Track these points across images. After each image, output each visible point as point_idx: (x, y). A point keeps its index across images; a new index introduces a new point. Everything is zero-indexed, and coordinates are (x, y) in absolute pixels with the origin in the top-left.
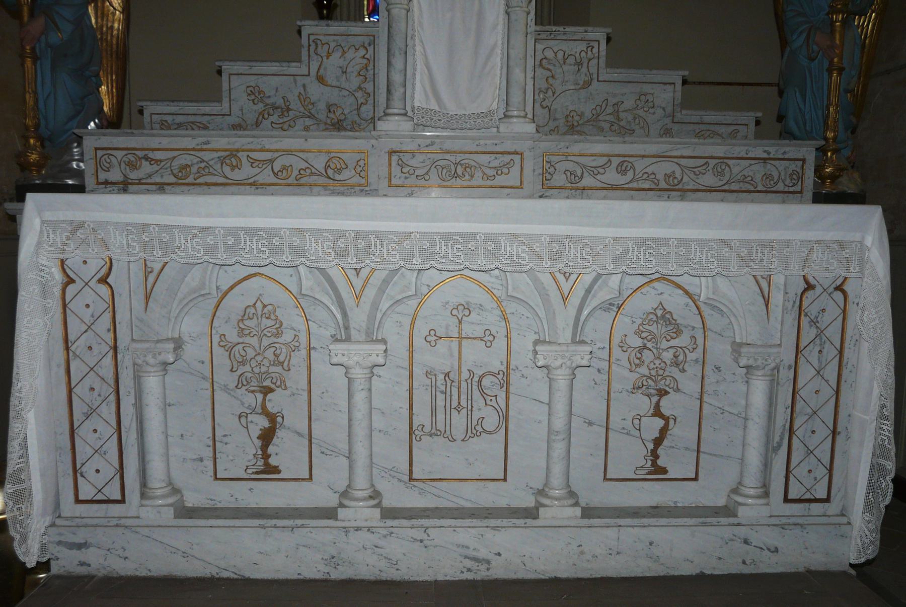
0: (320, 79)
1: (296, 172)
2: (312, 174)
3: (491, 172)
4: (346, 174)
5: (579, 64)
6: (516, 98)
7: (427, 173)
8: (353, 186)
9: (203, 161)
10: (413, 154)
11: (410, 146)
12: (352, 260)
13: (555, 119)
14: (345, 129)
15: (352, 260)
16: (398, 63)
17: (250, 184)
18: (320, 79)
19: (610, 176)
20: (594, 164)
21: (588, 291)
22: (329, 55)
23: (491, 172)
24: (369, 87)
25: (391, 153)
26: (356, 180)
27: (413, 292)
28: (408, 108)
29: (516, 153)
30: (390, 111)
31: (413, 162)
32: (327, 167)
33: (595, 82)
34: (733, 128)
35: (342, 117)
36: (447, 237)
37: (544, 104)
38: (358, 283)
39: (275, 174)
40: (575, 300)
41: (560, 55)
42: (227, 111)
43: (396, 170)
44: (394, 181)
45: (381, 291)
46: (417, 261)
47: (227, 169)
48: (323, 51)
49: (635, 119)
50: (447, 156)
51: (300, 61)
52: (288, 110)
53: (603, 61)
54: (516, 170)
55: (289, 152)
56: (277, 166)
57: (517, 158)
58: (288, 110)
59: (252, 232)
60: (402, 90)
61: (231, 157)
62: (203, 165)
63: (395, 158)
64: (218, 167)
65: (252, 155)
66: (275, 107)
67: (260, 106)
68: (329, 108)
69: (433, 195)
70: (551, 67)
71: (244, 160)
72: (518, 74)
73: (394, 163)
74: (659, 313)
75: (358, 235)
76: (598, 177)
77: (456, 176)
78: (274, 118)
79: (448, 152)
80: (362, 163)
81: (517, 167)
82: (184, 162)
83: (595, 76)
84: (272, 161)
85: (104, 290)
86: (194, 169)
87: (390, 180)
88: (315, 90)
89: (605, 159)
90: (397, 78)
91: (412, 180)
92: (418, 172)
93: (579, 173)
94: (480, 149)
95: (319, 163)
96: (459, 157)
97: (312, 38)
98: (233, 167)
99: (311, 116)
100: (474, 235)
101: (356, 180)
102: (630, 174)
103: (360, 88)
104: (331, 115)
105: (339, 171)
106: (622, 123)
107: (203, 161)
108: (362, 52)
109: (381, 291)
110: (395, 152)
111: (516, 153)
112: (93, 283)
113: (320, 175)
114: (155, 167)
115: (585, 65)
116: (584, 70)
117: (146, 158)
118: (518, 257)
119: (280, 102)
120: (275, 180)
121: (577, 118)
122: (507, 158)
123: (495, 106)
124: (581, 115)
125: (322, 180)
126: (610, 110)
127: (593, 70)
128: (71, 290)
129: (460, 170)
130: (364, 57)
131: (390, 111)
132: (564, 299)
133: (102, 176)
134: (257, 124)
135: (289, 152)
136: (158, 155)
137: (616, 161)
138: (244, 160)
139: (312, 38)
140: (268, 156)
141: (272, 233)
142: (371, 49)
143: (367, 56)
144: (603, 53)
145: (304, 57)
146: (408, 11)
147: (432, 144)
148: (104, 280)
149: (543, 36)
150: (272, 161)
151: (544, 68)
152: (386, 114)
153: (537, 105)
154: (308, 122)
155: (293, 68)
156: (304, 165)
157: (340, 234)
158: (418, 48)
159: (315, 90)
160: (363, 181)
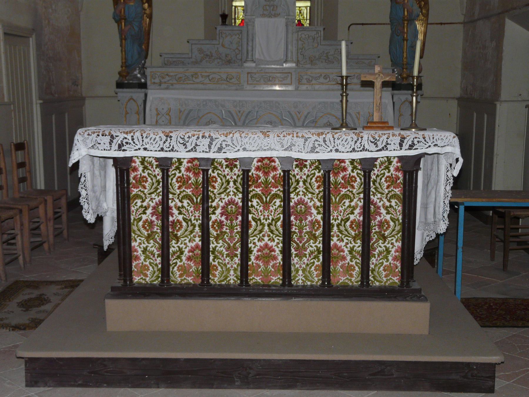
0: (223, 46)
1: (217, 80)
2: (222, 80)
3: (281, 79)
4: (233, 80)
5: (314, 39)
6: (289, 55)
7: (260, 80)
8: (235, 84)
9: (186, 76)
10: (255, 73)
11: (254, 71)
12: (238, 108)
13: (306, 59)
14: (232, 63)
15: (238, 108)
16: (250, 44)
17: (202, 84)
18: (223, 46)
19: (322, 80)
20: (316, 76)
21: (306, 117)
22: (226, 37)
23: (281, 79)
24: (240, 48)
25: (248, 73)
26: (237, 82)
27: (255, 117)
28: (254, 58)
29: (289, 73)
30: (248, 59)
31: (255, 76)
32: (227, 78)
33: (319, 45)
34: (369, 60)
35: (231, 59)
36: (265, 102)
37: (302, 53)
38: (240, 115)
39: (210, 80)
40: (302, 120)
41: (307, 36)
42: (190, 56)
43: (250, 78)
44: (249, 83)
45: (246, 117)
46: (256, 109)
47: (194, 79)
48: (224, 36)
49: (334, 58)
50: (267, 74)
51: (216, 40)
52: (212, 56)
53: (322, 38)
54: (289, 79)
55: (214, 73)
56: (211, 77)
57: (290, 75)
58: (212, 56)
59: (210, 101)
60: (252, 53)
61: (195, 75)
62: (186, 77)
63: (249, 75)
64: (191, 78)
65: (202, 74)
66: (207, 55)
67: (202, 55)
68: (226, 56)
69: (281, 362)
70: (304, 40)
71: (200, 76)
72: (290, 47)
73: (249, 76)
74: (328, 124)
75: (240, 101)
76: (318, 80)
77: (270, 80)
78: (207, 59)
79: (267, 73)
80: (238, 77)
81: (290, 78)
82: (179, 76)
83: (319, 43)
84: (209, 76)
85: (168, 117)
86: (183, 79)
87: (248, 82)
88: (221, 50)
89: (320, 75)
90: (250, 48)
91: (255, 82)
92: (257, 79)
93: (311, 79)
94: (277, 72)
95: (224, 77)
96: (271, 74)
97: (220, 31)
98: (196, 78)
99: (220, 59)
100: (272, 101)
101: (237, 82)
102: (328, 79)
103: (237, 49)
104: (227, 58)
105: (231, 79)
106: (329, 60)
107: (186, 76)
108: (238, 36)
109: (246, 117)
110: (250, 73)
111: (289, 73)
112: (165, 115)
113: (225, 80)
114: (171, 78)
115: (316, 39)
116: (316, 41)
117: (167, 75)
118: (285, 107)
119: (209, 53)
120: (210, 82)
121: (313, 58)
122: (286, 75)
123: (282, 57)
124: (315, 57)
125: (225, 82)
126: (325, 55)
127: (319, 41)
128: (159, 117)
129: (271, 79)
130: (238, 38)
131: (248, 59)
132: (299, 119)
133: (153, 81)
134: (201, 61)
135: (214, 73)
136: (171, 74)
137: (323, 75)
138: (200, 76)
139: (220, 31)
140: (208, 74)
141: (215, 101)
142: (241, 36)
143: (240, 37)
144: (322, 35)
145: (218, 38)
146: (253, 26)
147: (262, 70)
148: (168, 114)
149: (301, 29)
150: (209, 76)
151: (301, 41)
152: (246, 61)
153: (299, 54)
154: (219, 60)
155: (214, 42)
156: (219, 77)
157: (235, 101)
158: (257, 39)
159: (221, 50)
160: (239, 83)
